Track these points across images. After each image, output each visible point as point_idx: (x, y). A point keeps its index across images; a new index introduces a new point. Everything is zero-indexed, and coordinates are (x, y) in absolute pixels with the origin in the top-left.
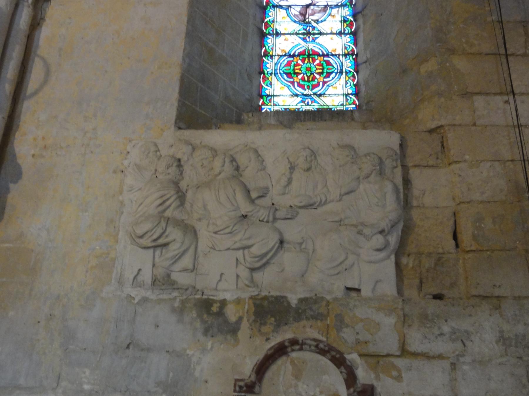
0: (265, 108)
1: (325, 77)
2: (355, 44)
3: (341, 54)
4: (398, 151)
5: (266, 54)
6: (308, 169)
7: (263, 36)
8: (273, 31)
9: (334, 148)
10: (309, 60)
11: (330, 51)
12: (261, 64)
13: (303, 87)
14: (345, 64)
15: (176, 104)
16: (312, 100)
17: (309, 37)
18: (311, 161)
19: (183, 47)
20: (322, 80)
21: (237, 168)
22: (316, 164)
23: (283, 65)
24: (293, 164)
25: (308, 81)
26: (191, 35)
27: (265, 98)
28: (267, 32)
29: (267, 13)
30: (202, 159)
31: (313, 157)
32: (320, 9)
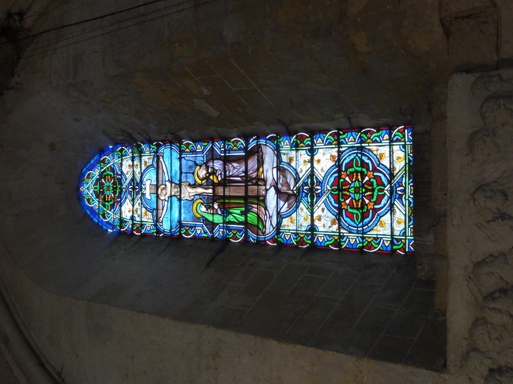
0: (409, 247)
1: (368, 170)
2: (326, 132)
3: (337, 149)
4: (477, 75)
5: (337, 244)
6: (504, 194)
7: (314, 247)
8: (307, 235)
9: (473, 161)
10: (345, 190)
11: (334, 163)
12: (351, 251)
13: (380, 198)
14: (350, 144)
15: (411, 369)
16: (397, 185)
17: (318, 189)
18: (492, 190)
19: (335, 353)
20: (372, 173)
21: (503, 291)
22: (496, 184)
23: (352, 223)
24: (496, 215)
25: (373, 190)
26: (318, 340)
27: (395, 247)
28: (310, 242)
29: (286, 242)
30: (490, 338)
31: (486, 188)
32: (281, 177)
